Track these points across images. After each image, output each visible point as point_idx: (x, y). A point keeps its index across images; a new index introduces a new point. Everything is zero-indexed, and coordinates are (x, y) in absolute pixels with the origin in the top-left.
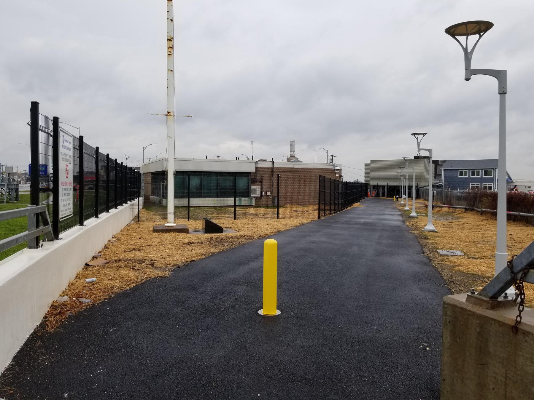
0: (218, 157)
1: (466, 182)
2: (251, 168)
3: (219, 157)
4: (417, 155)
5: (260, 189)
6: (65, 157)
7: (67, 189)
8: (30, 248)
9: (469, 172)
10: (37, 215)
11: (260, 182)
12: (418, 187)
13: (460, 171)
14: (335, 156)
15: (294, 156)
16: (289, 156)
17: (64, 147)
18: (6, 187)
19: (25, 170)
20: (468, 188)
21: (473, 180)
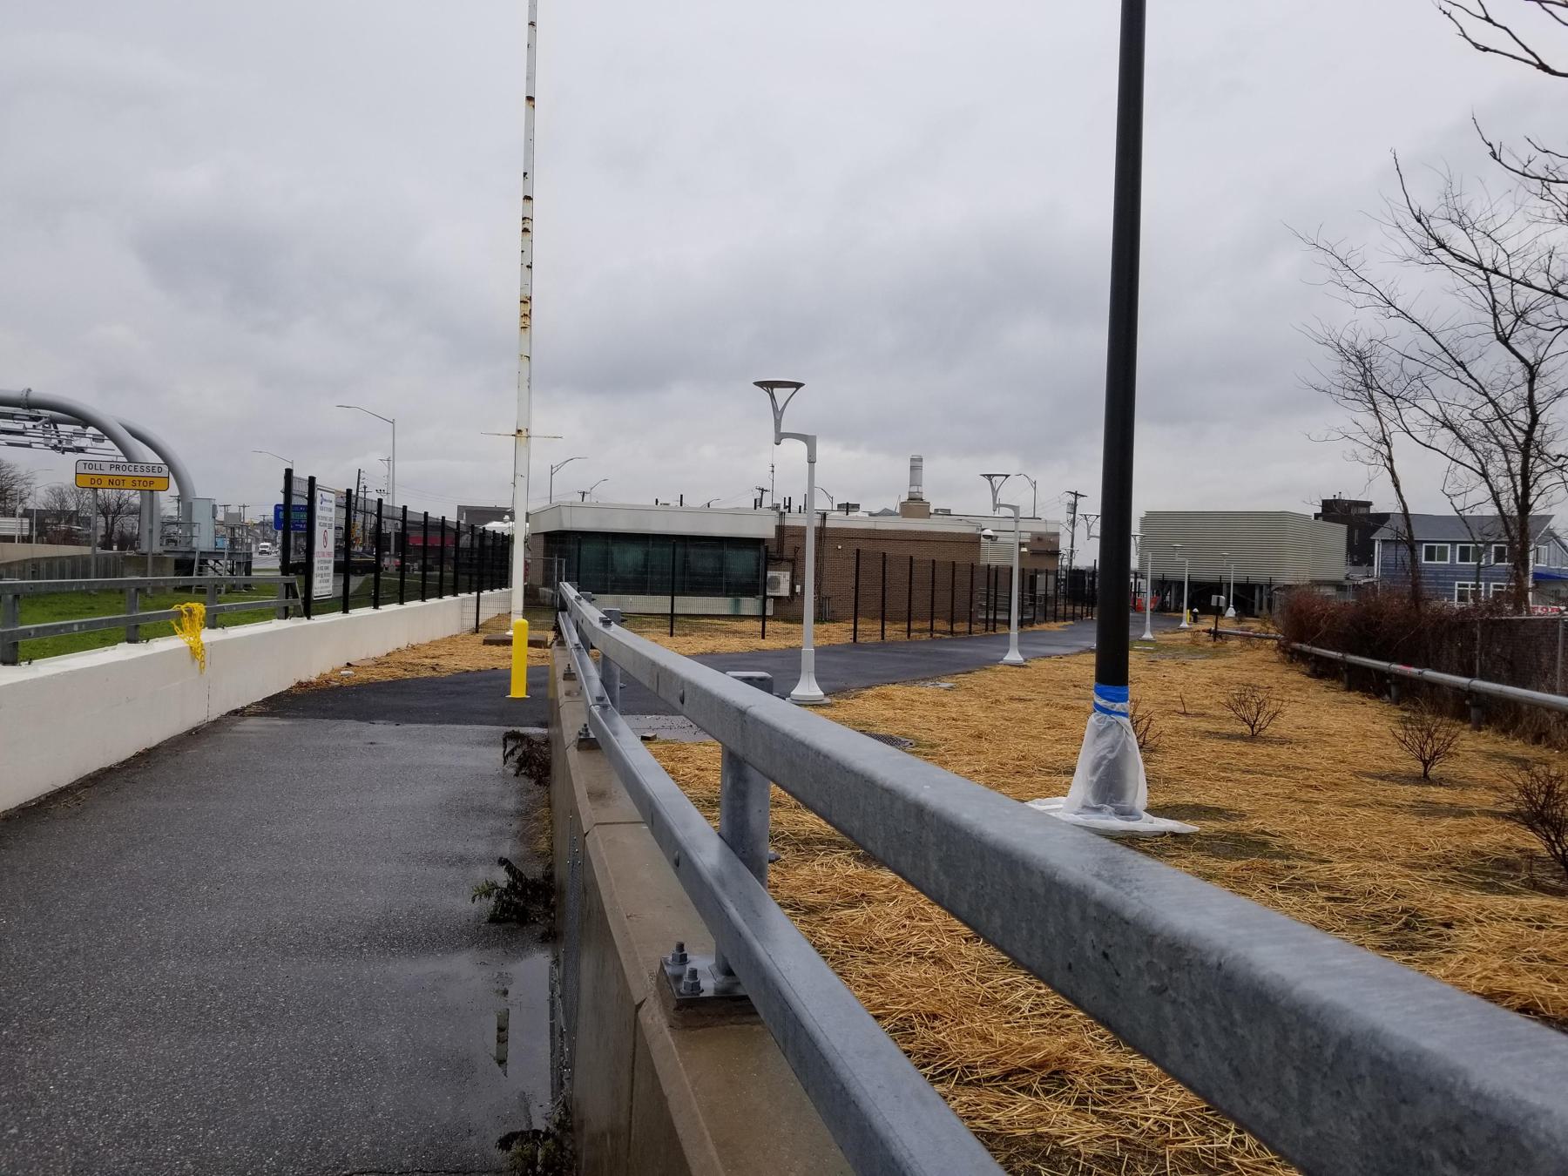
0: (763, 490)
1: (1445, 578)
2: (763, 527)
3: (766, 491)
4: (1332, 498)
5: (788, 577)
6: (323, 521)
7: (325, 562)
8: (279, 618)
9: (1453, 551)
10: (287, 585)
11: (789, 561)
12: (1273, 588)
13: (1426, 546)
14: (1083, 496)
15: (920, 497)
16: (905, 498)
17: (322, 509)
18: (226, 557)
19: (264, 516)
20: (1447, 596)
21: (1463, 573)
